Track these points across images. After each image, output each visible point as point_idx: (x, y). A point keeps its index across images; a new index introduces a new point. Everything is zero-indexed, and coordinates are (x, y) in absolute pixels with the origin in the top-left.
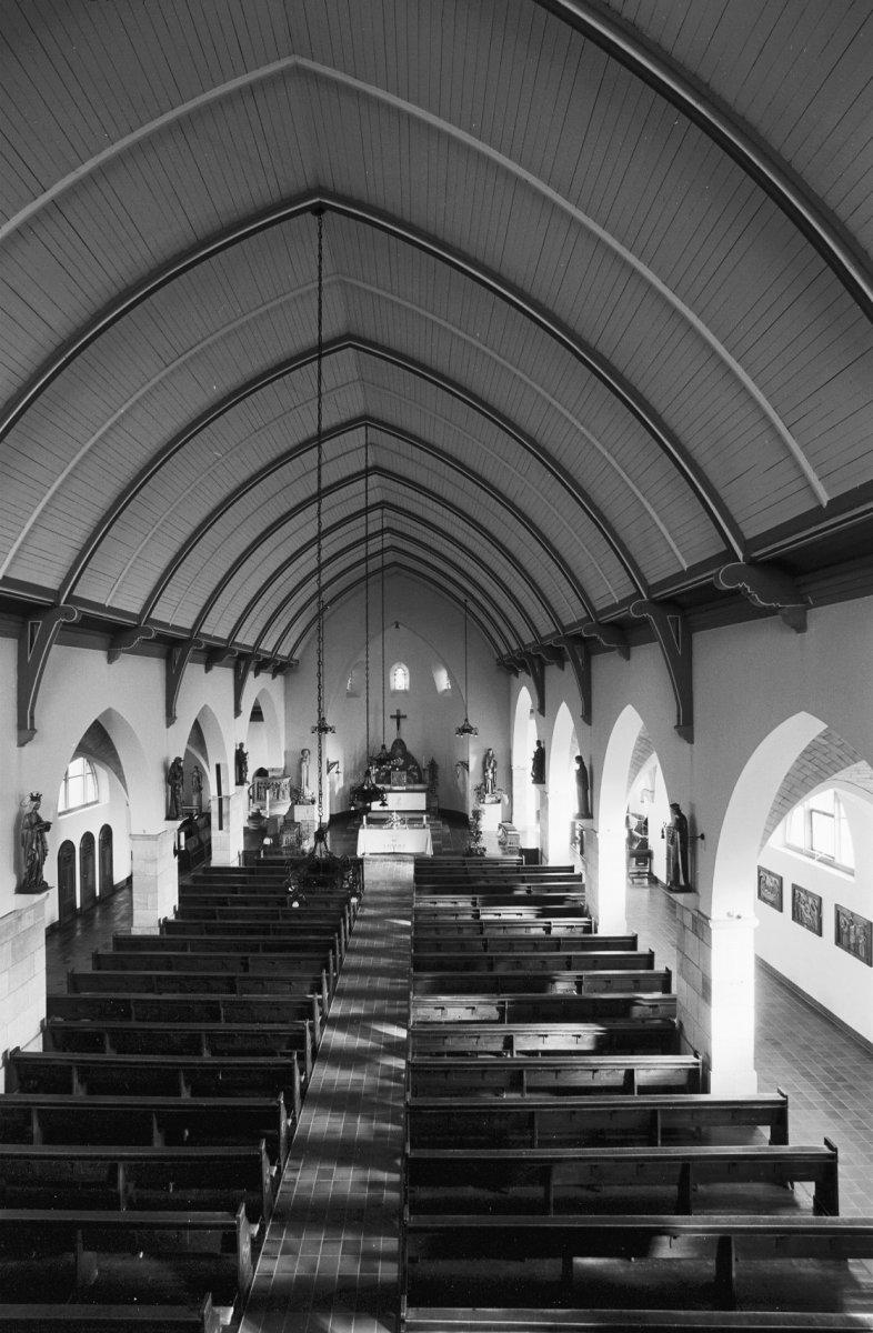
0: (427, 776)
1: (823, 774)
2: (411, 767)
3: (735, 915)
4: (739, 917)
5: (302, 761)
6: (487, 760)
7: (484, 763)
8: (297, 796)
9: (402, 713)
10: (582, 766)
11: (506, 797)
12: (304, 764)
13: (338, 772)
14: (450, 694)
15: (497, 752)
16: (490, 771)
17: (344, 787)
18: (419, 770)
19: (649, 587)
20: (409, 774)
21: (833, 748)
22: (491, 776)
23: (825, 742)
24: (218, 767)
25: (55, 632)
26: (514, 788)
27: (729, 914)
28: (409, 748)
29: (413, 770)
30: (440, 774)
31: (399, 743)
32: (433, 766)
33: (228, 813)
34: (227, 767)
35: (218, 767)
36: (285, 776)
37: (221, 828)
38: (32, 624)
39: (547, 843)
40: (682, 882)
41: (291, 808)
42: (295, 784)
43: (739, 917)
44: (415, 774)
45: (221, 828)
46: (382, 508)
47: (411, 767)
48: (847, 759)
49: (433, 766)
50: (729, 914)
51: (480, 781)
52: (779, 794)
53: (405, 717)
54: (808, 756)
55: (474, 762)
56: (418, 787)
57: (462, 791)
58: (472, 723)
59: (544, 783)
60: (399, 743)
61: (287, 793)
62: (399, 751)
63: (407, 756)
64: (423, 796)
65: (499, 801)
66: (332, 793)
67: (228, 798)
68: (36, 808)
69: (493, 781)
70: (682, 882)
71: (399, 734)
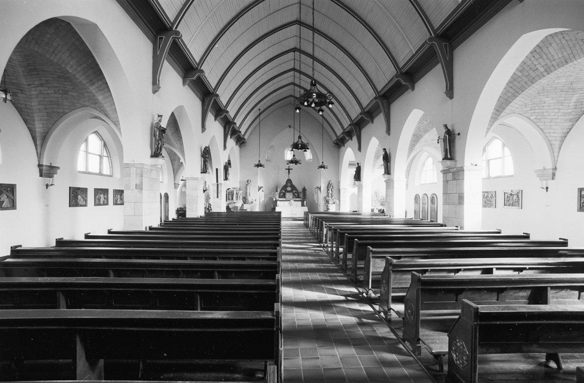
0: (301, 195)
1: (516, 94)
2: (294, 191)
3: (475, 164)
4: (476, 165)
5: (247, 185)
6: (329, 185)
7: (328, 187)
8: (245, 200)
9: (290, 168)
10: (386, 153)
11: (337, 201)
12: (248, 186)
13: (263, 191)
14: (312, 161)
15: (333, 182)
16: (330, 190)
17: (264, 201)
18: (298, 193)
19: (435, 31)
20: (294, 194)
21: (523, 78)
22: (331, 192)
23: (520, 74)
24: (217, 169)
25: (166, 53)
26: (341, 197)
27: (472, 164)
28: (294, 183)
29: (296, 193)
30: (307, 192)
31: (289, 181)
32: (304, 190)
33: (221, 191)
34: (220, 169)
35: (217, 169)
36: (240, 190)
37: (226, 179)
38: (160, 38)
39: (361, 206)
40: (449, 157)
41: (242, 205)
42: (244, 196)
43: (476, 165)
44: (296, 194)
45: (226, 179)
46: (294, 52)
47: (294, 191)
48: (529, 83)
49: (304, 190)
50: (472, 164)
51: (326, 195)
52: (495, 109)
53: (292, 169)
54: (511, 85)
55: (323, 187)
56: (297, 199)
57: (316, 202)
58: (325, 164)
59: (360, 181)
60: (289, 181)
61: (241, 198)
62: (289, 184)
63: (293, 188)
64: (300, 202)
65: (334, 203)
66: (260, 202)
67: (221, 184)
68: (160, 121)
69: (332, 195)
70: (449, 157)
71: (289, 177)
